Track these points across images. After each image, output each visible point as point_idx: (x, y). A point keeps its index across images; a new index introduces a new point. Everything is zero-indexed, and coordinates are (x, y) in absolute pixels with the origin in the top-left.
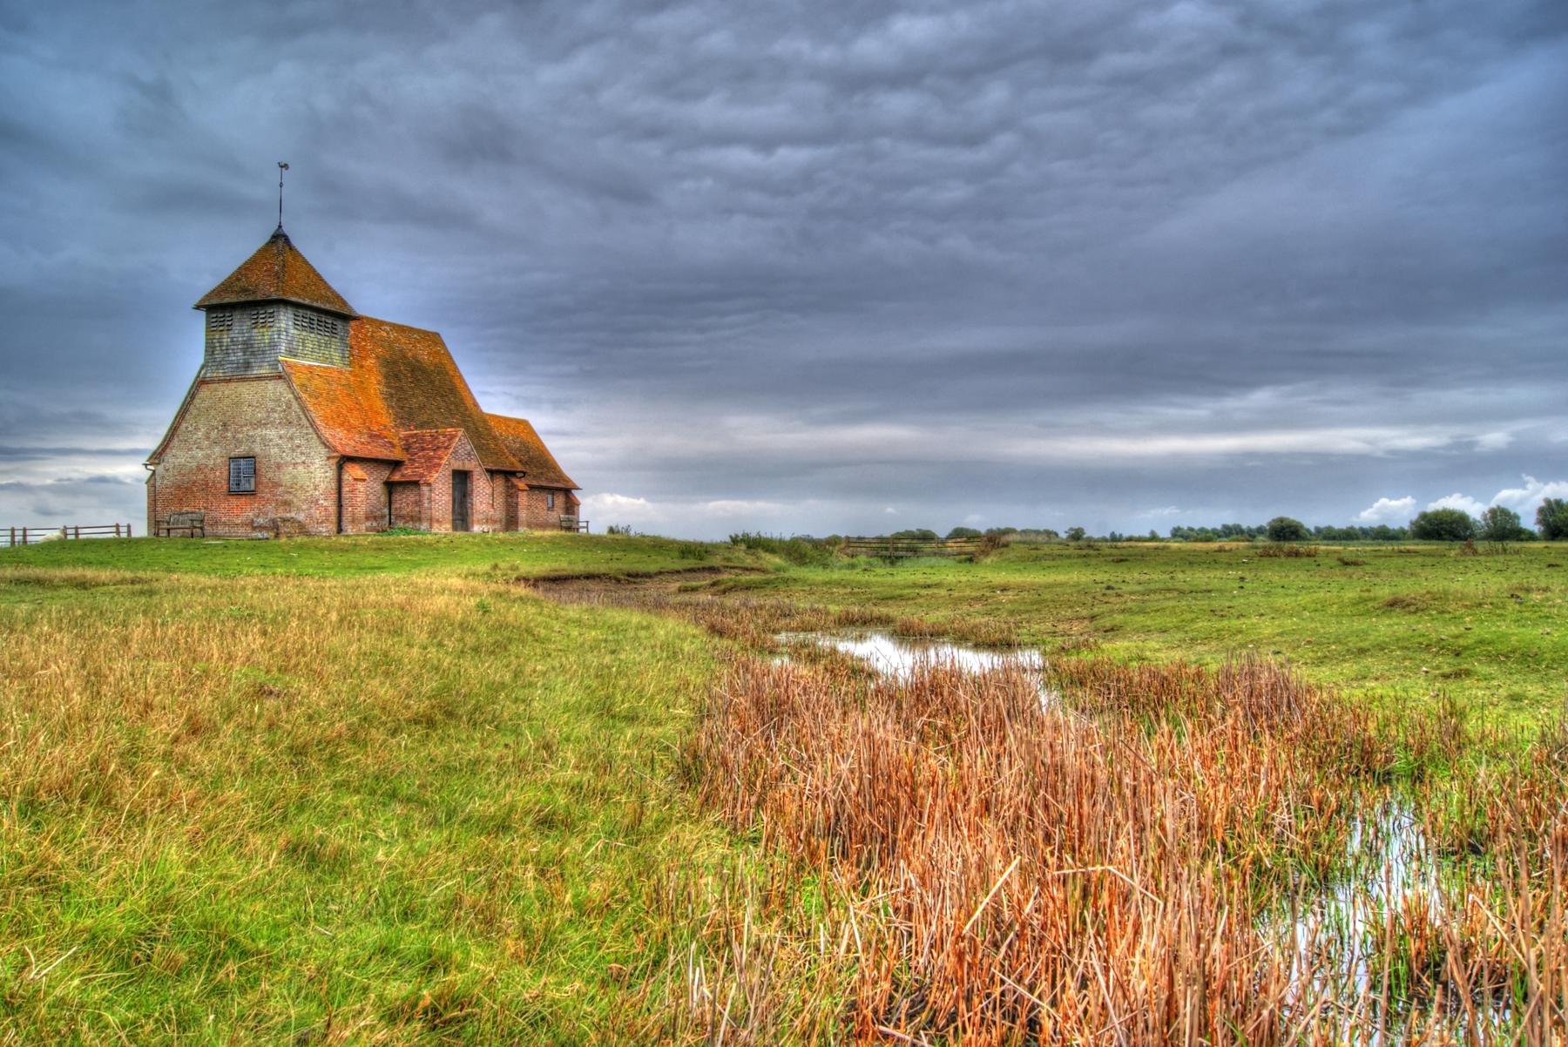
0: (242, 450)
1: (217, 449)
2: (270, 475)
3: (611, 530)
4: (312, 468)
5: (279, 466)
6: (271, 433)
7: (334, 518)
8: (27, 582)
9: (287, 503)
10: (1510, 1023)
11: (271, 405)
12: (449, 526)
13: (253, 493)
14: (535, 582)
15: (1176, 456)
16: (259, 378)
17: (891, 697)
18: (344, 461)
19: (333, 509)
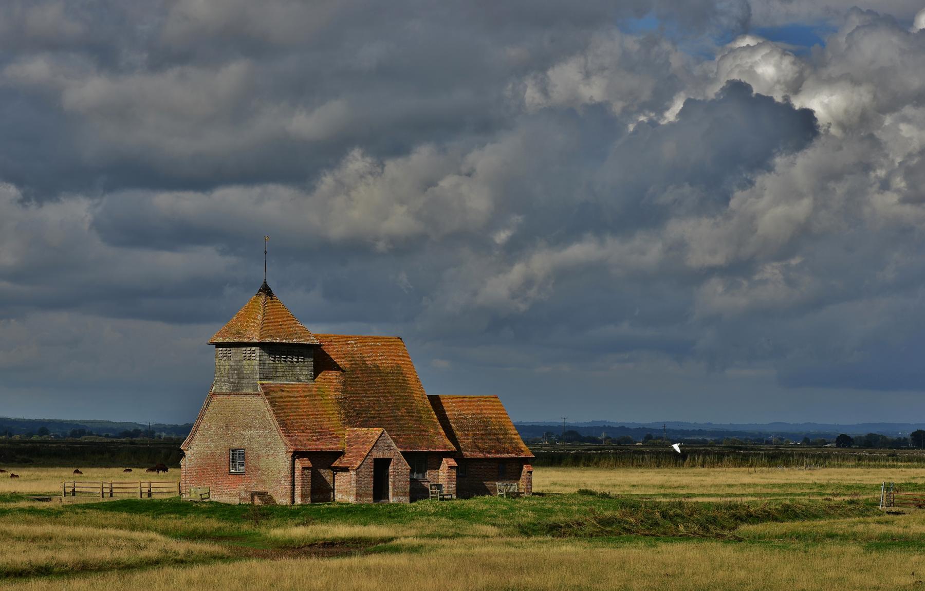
0: (236, 445)
1: (222, 442)
2: (253, 462)
3: (751, 183)
4: (277, 459)
5: (258, 456)
6: (254, 433)
7: (289, 494)
8: (34, 539)
9: (263, 481)
10: (498, 507)
11: (253, 413)
12: (371, 499)
13: (243, 474)
14: (396, 538)
15: (44, 473)
16: (246, 395)
17: (528, 568)
18: (297, 455)
19: (289, 487)
